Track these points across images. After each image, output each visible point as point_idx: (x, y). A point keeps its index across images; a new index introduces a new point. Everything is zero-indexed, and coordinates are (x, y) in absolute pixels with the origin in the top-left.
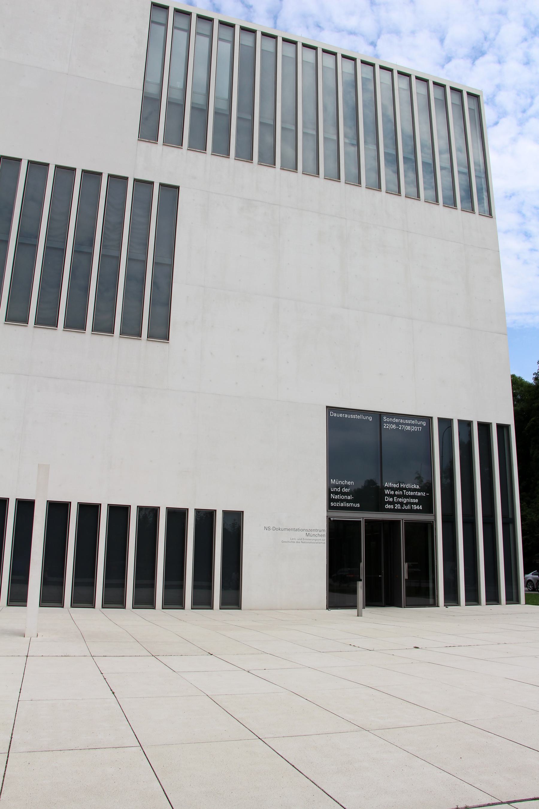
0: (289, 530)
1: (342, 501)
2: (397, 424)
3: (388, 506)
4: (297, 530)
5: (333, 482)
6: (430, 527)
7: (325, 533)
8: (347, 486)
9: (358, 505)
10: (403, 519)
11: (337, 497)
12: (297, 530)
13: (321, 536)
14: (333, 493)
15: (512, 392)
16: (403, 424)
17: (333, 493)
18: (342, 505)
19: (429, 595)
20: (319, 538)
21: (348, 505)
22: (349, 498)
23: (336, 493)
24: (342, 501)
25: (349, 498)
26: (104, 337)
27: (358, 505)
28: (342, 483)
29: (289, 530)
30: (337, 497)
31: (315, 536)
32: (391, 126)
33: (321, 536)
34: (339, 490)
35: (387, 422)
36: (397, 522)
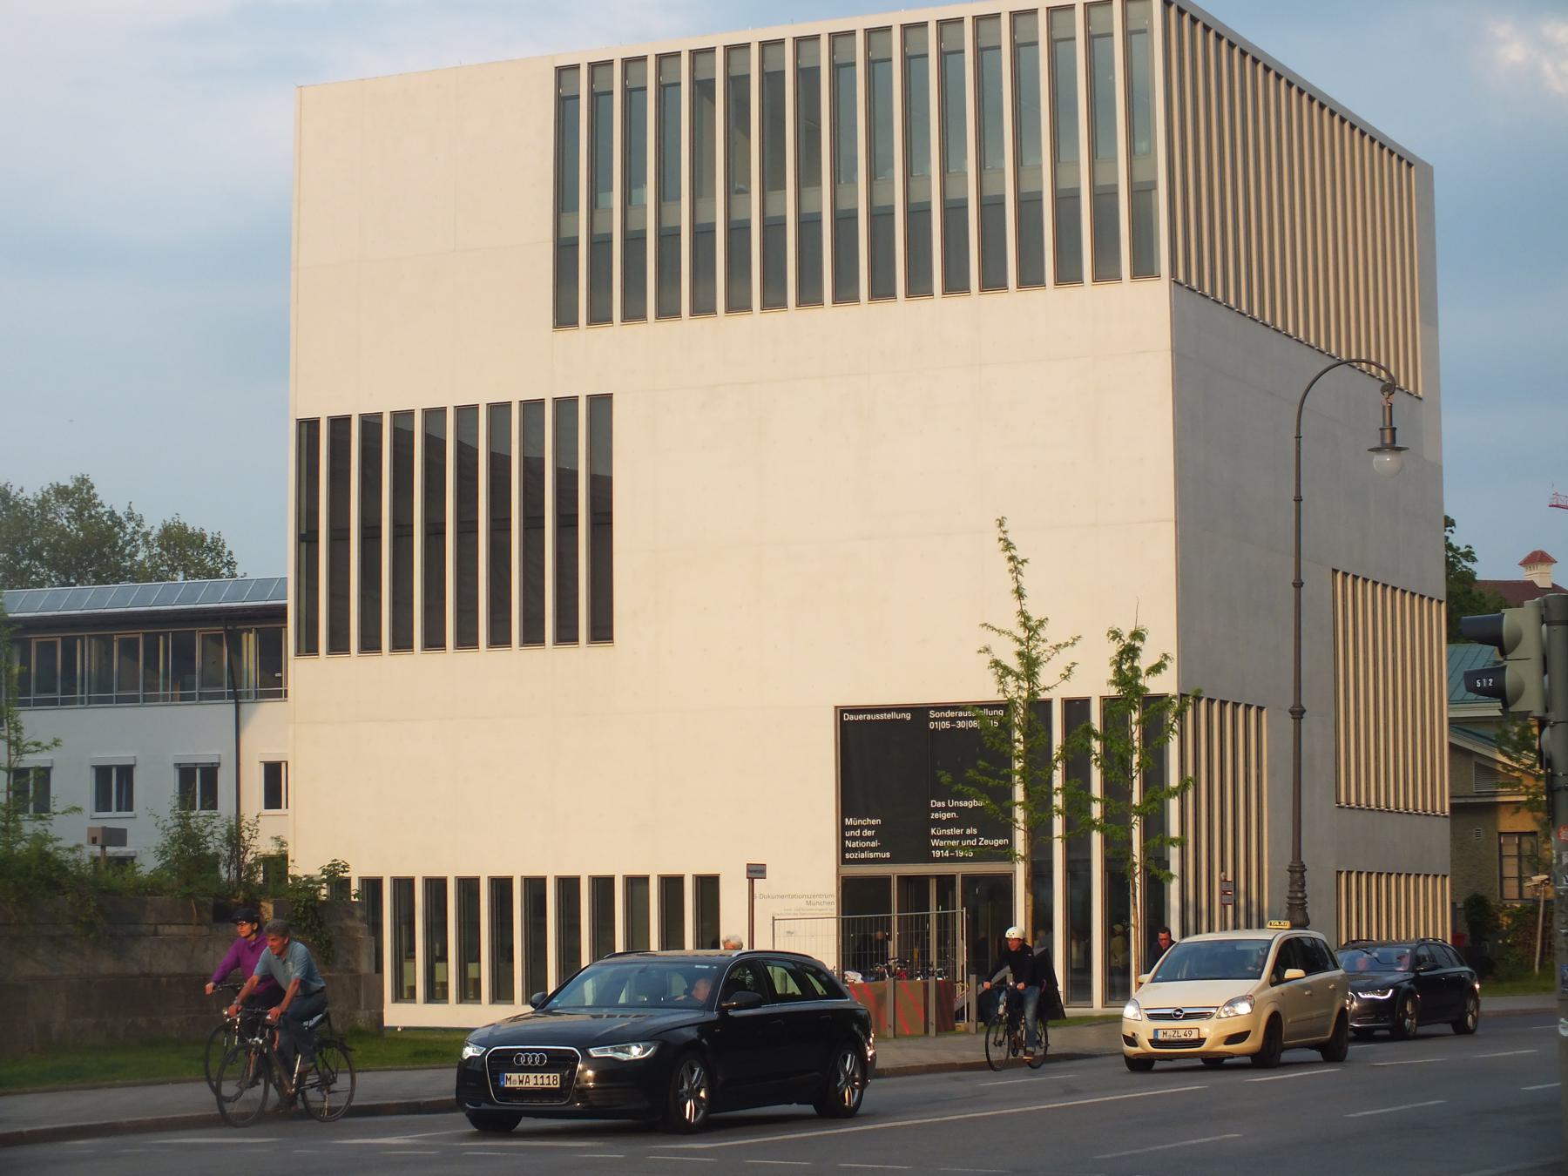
0: (782, 897)
1: (862, 850)
2: (953, 720)
3: (937, 854)
4: (793, 897)
5: (848, 822)
6: (1003, 886)
7: (835, 900)
8: (869, 827)
9: (888, 855)
10: (894, 874)
11: (855, 845)
12: (793, 897)
13: (829, 903)
14: (849, 838)
15: (30, 768)
16: (962, 719)
17: (849, 838)
18: (863, 856)
19: (513, 999)
20: (825, 906)
21: (872, 855)
22: (874, 844)
23: (853, 839)
24: (862, 850)
25: (874, 844)
26: (127, 709)
27: (888, 855)
28: (863, 822)
29: (782, 897)
30: (855, 845)
31: (820, 904)
32: (1141, 146)
33: (829, 903)
34: (857, 833)
35: (935, 720)
36: (886, 880)
